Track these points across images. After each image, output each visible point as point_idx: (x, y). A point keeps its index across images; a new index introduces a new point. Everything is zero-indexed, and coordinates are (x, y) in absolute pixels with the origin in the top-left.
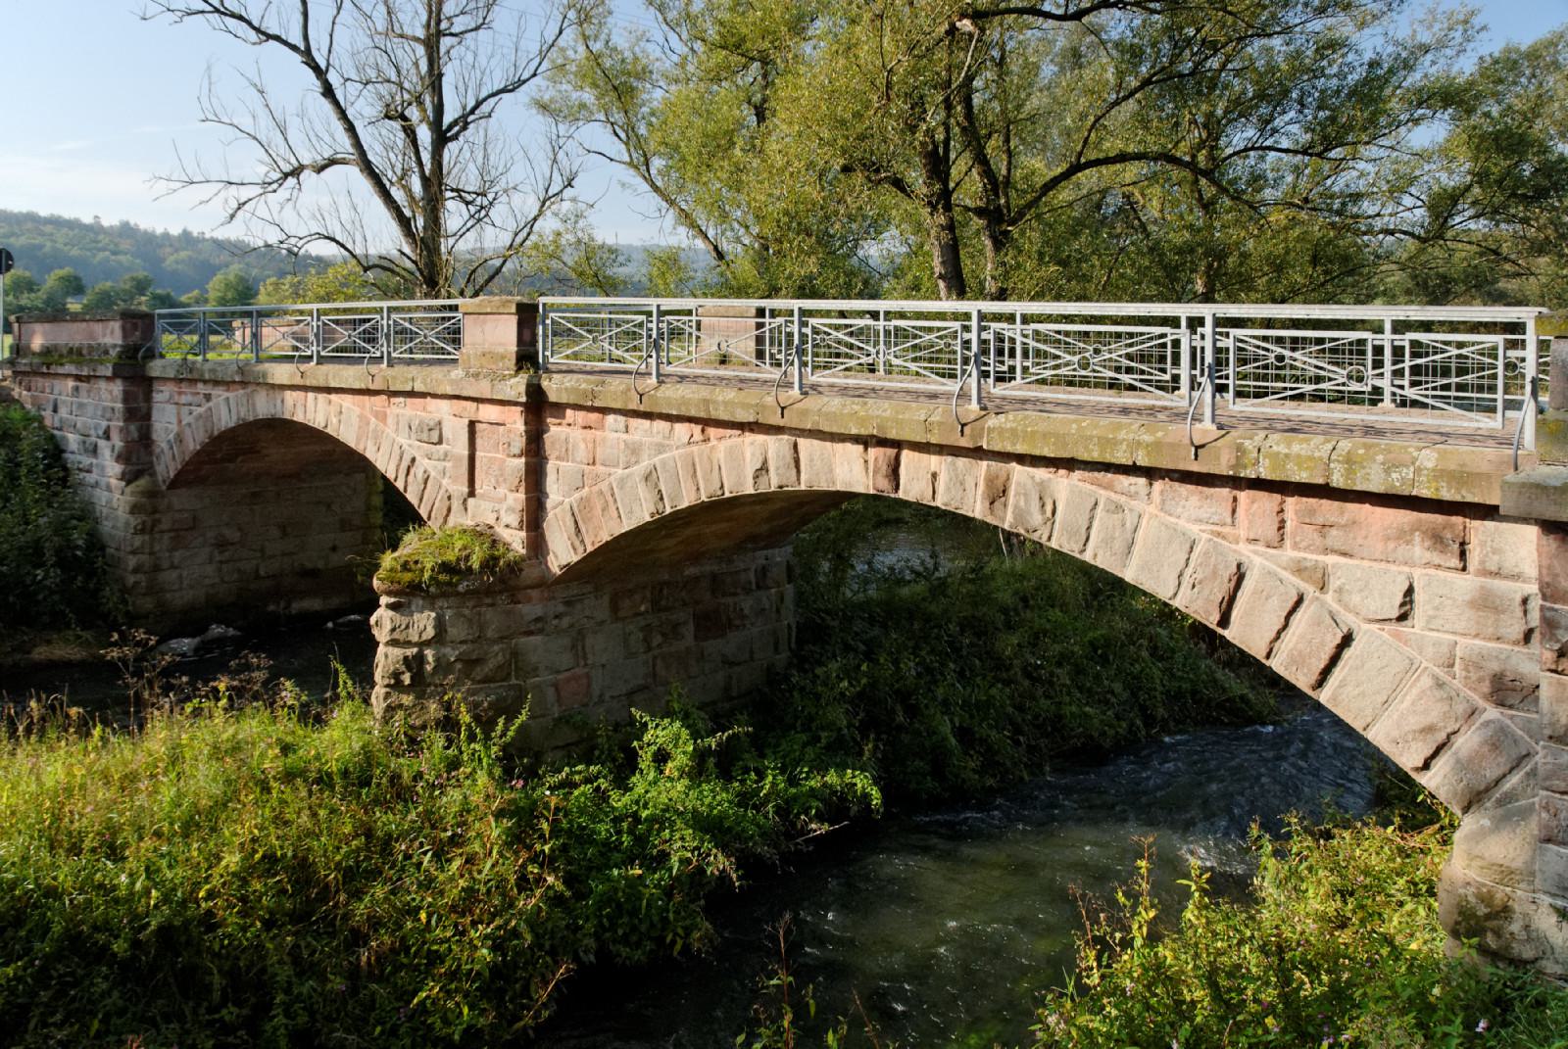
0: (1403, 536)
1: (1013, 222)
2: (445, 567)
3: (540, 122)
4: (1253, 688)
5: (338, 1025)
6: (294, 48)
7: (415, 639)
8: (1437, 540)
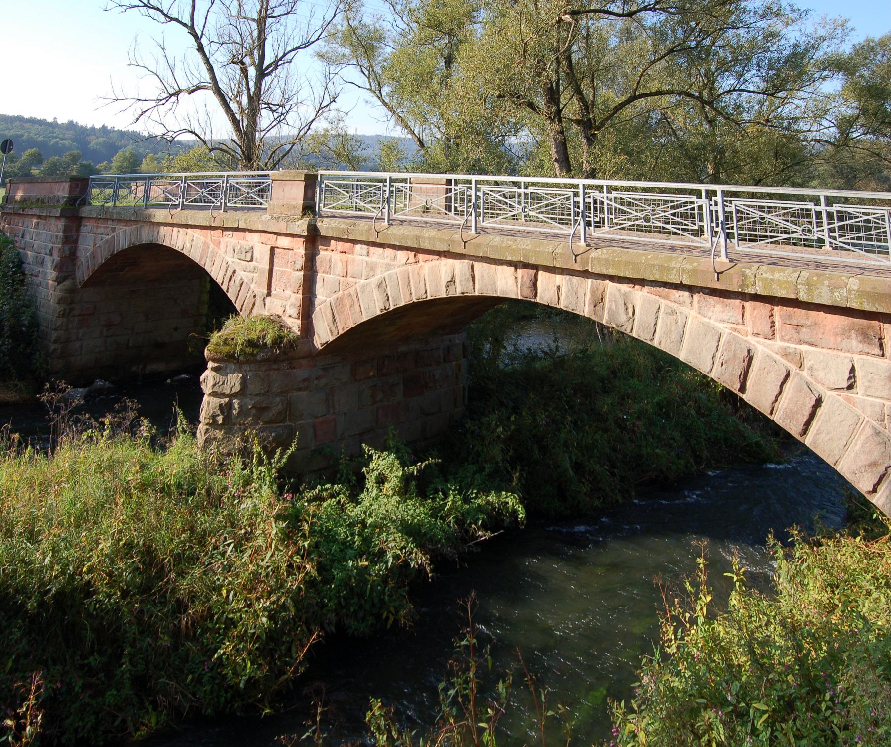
0: (845, 333)
1: (598, 129)
2: (250, 343)
3: (319, 65)
4: (763, 437)
5: (163, 673)
6: (185, 25)
7: (228, 392)
8: (865, 336)
